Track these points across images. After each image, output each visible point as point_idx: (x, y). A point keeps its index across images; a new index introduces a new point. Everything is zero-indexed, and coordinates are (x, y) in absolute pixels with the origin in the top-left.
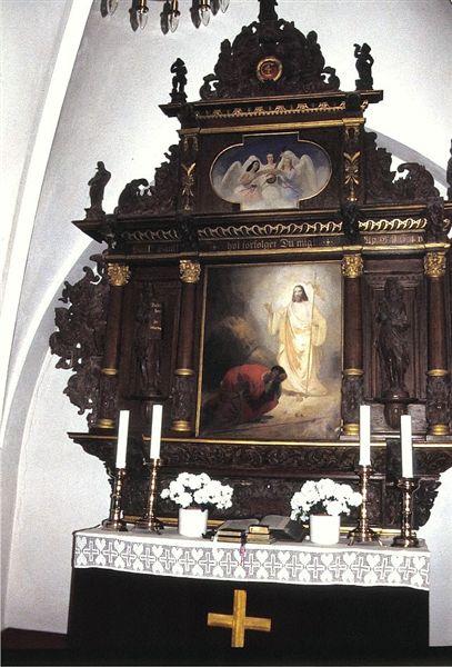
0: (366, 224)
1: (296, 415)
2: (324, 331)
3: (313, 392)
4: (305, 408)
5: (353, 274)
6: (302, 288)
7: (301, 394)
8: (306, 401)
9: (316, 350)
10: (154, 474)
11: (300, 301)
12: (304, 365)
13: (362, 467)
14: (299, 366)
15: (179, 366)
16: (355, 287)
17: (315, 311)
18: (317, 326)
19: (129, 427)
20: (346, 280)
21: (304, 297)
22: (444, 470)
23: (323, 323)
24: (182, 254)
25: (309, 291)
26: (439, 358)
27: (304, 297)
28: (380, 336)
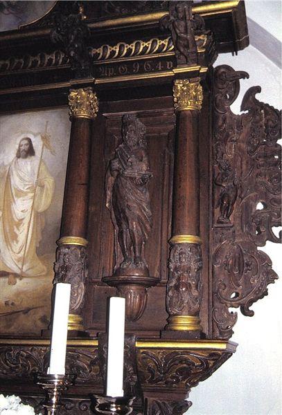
0: (100, 51)
1: (7, 303)
2: (50, 193)
3: (30, 272)
4: (18, 294)
5: (83, 114)
6: (29, 140)
7: (16, 275)
8: (20, 284)
9: (38, 215)
10: (54, 400)
11: (25, 157)
12: (21, 237)
13: (51, 377)
14: (15, 237)
15: (175, 231)
16: (84, 131)
17: (43, 168)
18: (42, 187)
19: (125, 323)
20: (74, 120)
21: (30, 152)
22: (195, 384)
23: (49, 182)
24: (177, 71)
25: (37, 144)
26: (187, 218)
27: (30, 152)
28: (113, 191)
